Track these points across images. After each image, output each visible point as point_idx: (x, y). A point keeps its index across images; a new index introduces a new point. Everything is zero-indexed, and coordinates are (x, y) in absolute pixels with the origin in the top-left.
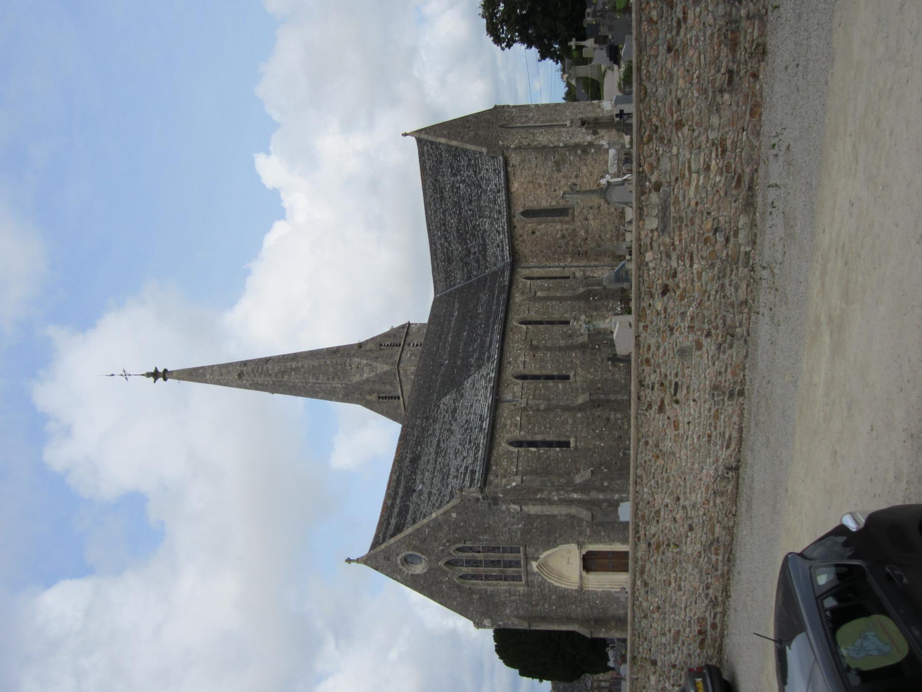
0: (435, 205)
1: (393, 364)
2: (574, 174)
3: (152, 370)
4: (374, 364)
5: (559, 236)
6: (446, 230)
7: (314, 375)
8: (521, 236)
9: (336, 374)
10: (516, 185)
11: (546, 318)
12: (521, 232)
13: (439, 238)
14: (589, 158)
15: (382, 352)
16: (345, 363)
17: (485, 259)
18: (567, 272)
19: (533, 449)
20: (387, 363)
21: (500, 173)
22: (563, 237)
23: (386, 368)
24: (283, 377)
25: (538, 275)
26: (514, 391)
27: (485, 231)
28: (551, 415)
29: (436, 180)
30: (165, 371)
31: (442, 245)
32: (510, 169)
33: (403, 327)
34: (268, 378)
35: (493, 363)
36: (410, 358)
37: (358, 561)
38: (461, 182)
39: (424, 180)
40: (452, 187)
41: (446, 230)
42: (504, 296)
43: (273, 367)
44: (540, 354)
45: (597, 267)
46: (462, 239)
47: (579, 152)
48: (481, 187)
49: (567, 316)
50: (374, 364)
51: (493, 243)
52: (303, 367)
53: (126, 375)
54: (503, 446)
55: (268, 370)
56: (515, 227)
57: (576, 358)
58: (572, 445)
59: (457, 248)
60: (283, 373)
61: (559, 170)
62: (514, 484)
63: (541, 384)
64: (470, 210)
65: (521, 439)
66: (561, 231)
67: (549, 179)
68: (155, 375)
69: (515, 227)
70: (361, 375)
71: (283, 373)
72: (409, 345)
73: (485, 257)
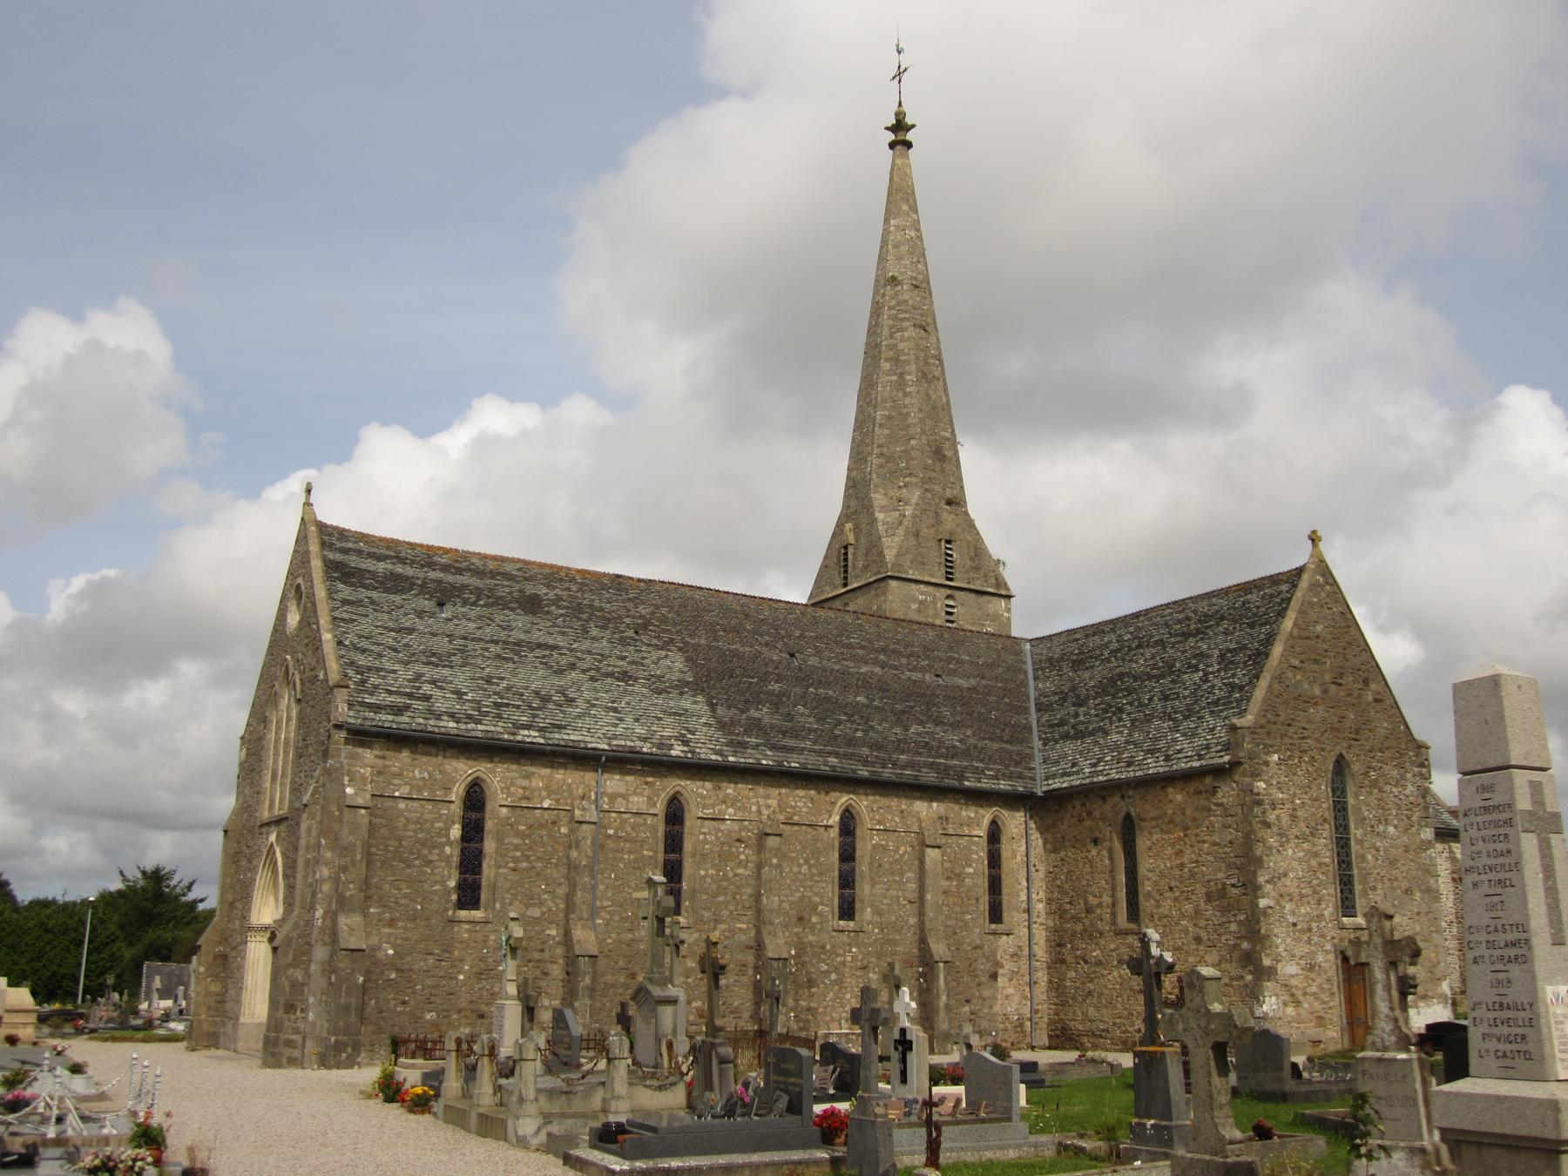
0: (1179, 622)
1: (897, 565)
2: (1203, 934)
3: (909, 120)
4: (901, 531)
5: (1092, 901)
6: (1130, 649)
7: (890, 417)
8: (1089, 813)
9: (889, 459)
10: (1179, 798)
11: (863, 867)
12: (1097, 814)
13: (1120, 640)
14: (1235, 970)
15: (933, 544)
16: (910, 475)
17: (1062, 738)
18: (1013, 917)
19: (456, 832)
20: (899, 555)
21: (1200, 757)
22: (1089, 910)
23: (890, 555)
24: (887, 360)
25: (1005, 853)
26: (639, 797)
27: (1106, 733)
28: (556, 874)
29: (1222, 618)
30: (909, 145)
31: (1106, 646)
32: (1208, 780)
33: (1000, 582)
34: (886, 332)
35: (716, 752)
36: (915, 600)
37: (308, 504)
38: (1206, 674)
39: (1226, 591)
40: (1202, 655)
41: (1130, 649)
42: (929, 777)
43: (908, 339)
44: (745, 853)
45: (1032, 984)
46: (1109, 686)
47: (1245, 945)
48: (1186, 718)
49: (866, 914)
50: (901, 531)
51: (1081, 753)
52: (906, 395)
53: (899, 74)
54: (463, 770)
55: (901, 330)
56: (1104, 799)
57: (732, 931)
58: (463, 914)
59: (1091, 678)
60: (896, 361)
61: (1209, 897)
62: (349, 790)
63: (655, 850)
64: (1150, 700)
65: (488, 808)
66: (1100, 905)
67: (1192, 875)
68: (900, 126)
69: (1104, 799)
70: (883, 509)
71: (896, 361)
72: (949, 597)
73: (1065, 737)
